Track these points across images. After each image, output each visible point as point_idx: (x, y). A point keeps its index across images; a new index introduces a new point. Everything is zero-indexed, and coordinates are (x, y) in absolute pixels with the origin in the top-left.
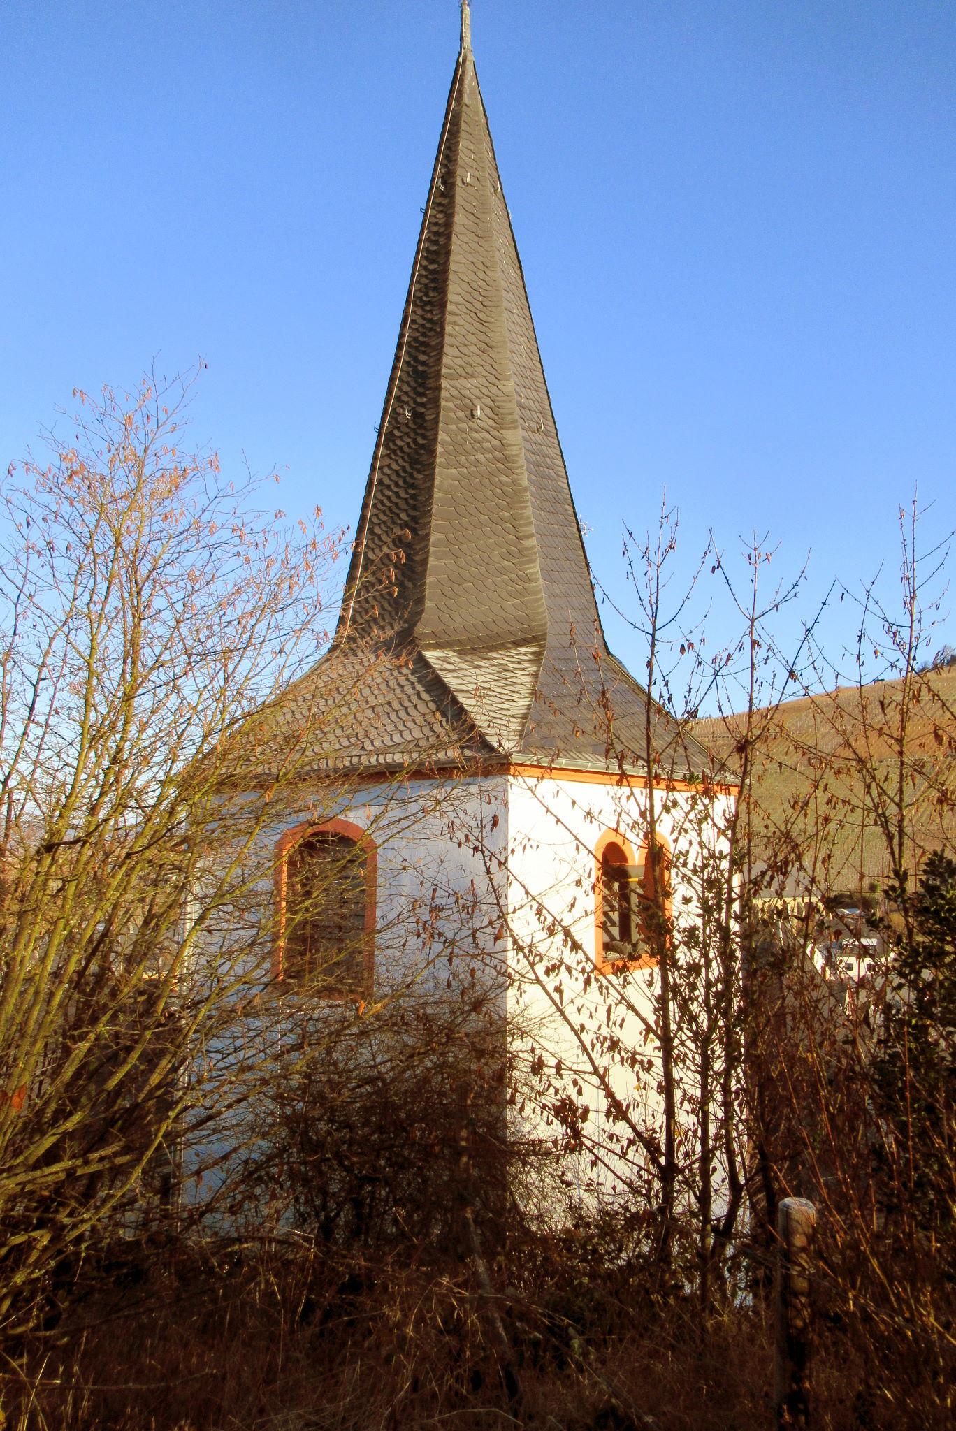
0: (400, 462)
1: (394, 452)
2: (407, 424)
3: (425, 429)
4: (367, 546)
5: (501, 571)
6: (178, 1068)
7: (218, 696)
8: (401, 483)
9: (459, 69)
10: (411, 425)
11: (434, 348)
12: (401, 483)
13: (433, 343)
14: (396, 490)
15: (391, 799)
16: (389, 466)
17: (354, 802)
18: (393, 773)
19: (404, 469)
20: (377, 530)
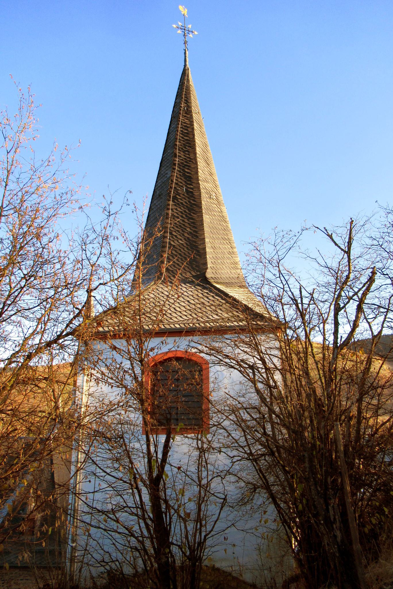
0: (182, 208)
1: (178, 204)
2: (183, 195)
3: (194, 197)
4: (169, 239)
5: (228, 258)
6: (228, 303)
7: (21, 421)
8: (184, 216)
9: (185, 73)
10: (186, 195)
11: (194, 168)
12: (184, 216)
13: (193, 166)
14: (159, 296)
15: (116, 470)
16: (176, 209)
17: (174, 353)
18: (194, 331)
19: (185, 211)
20: (174, 233)
